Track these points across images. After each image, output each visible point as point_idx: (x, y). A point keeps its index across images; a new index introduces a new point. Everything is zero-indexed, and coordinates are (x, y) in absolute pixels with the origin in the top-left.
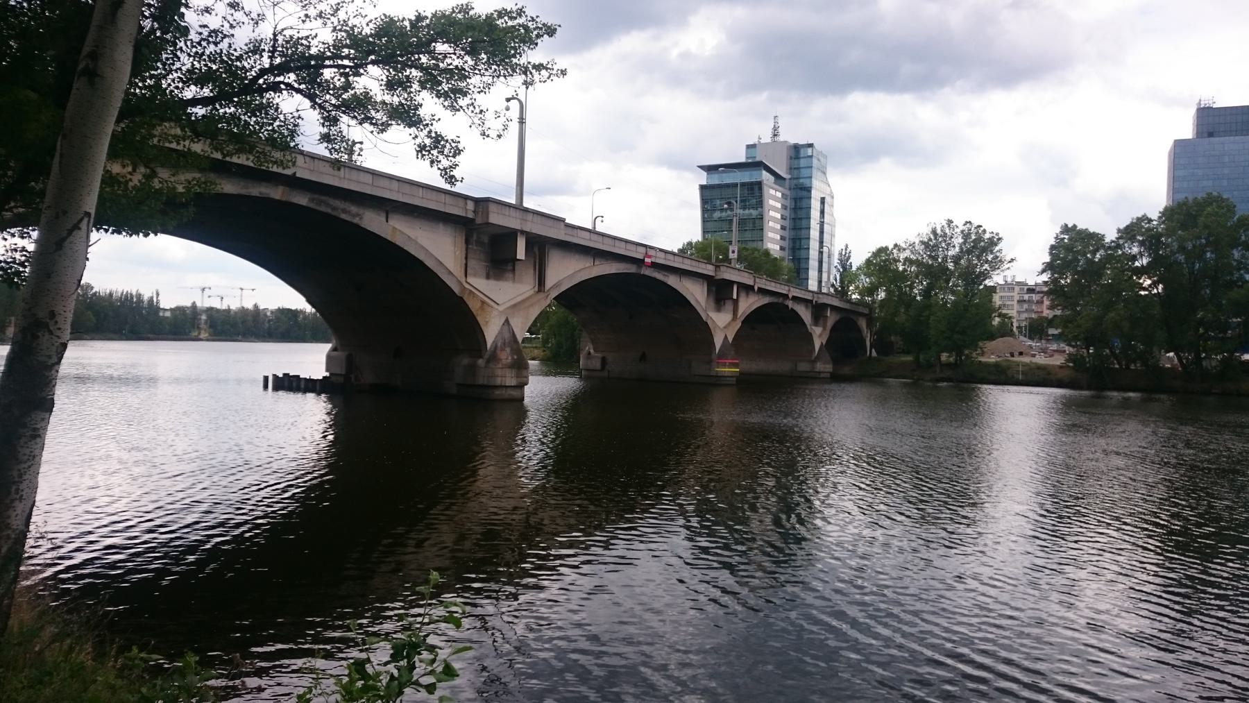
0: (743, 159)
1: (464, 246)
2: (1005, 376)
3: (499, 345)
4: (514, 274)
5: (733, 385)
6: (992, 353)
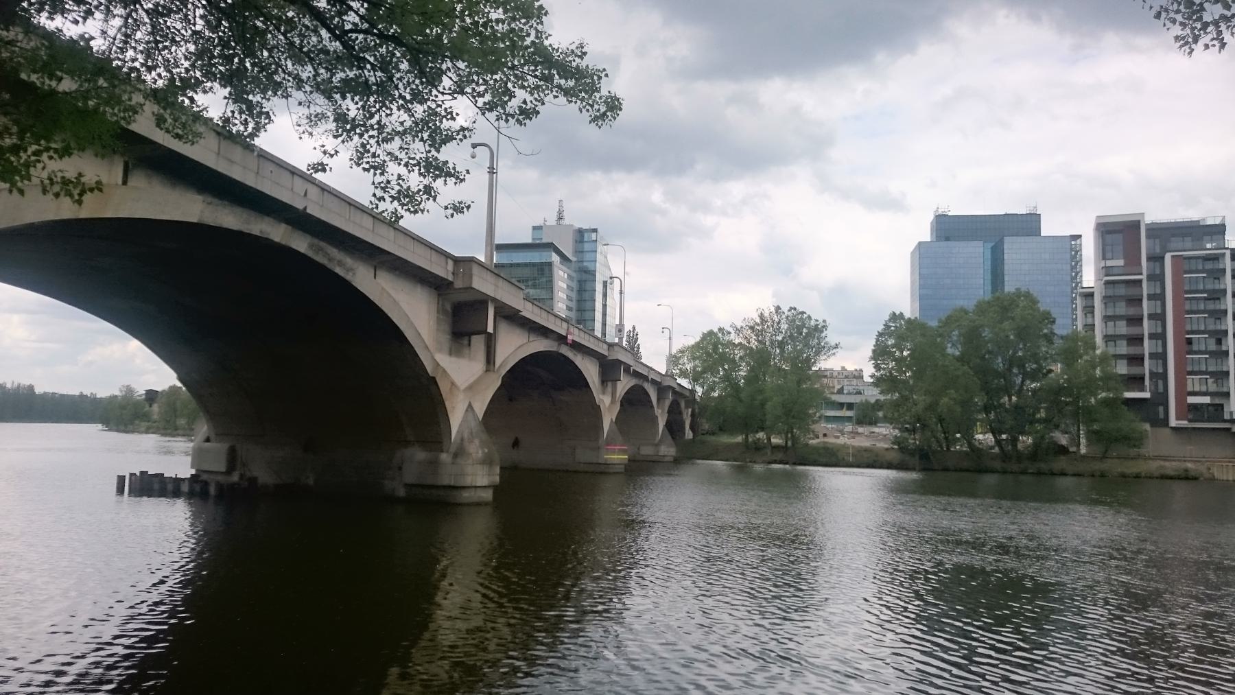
0: (529, 240)
2: (833, 458)
3: (466, 436)
4: (470, 349)
5: (622, 473)
6: (883, 434)
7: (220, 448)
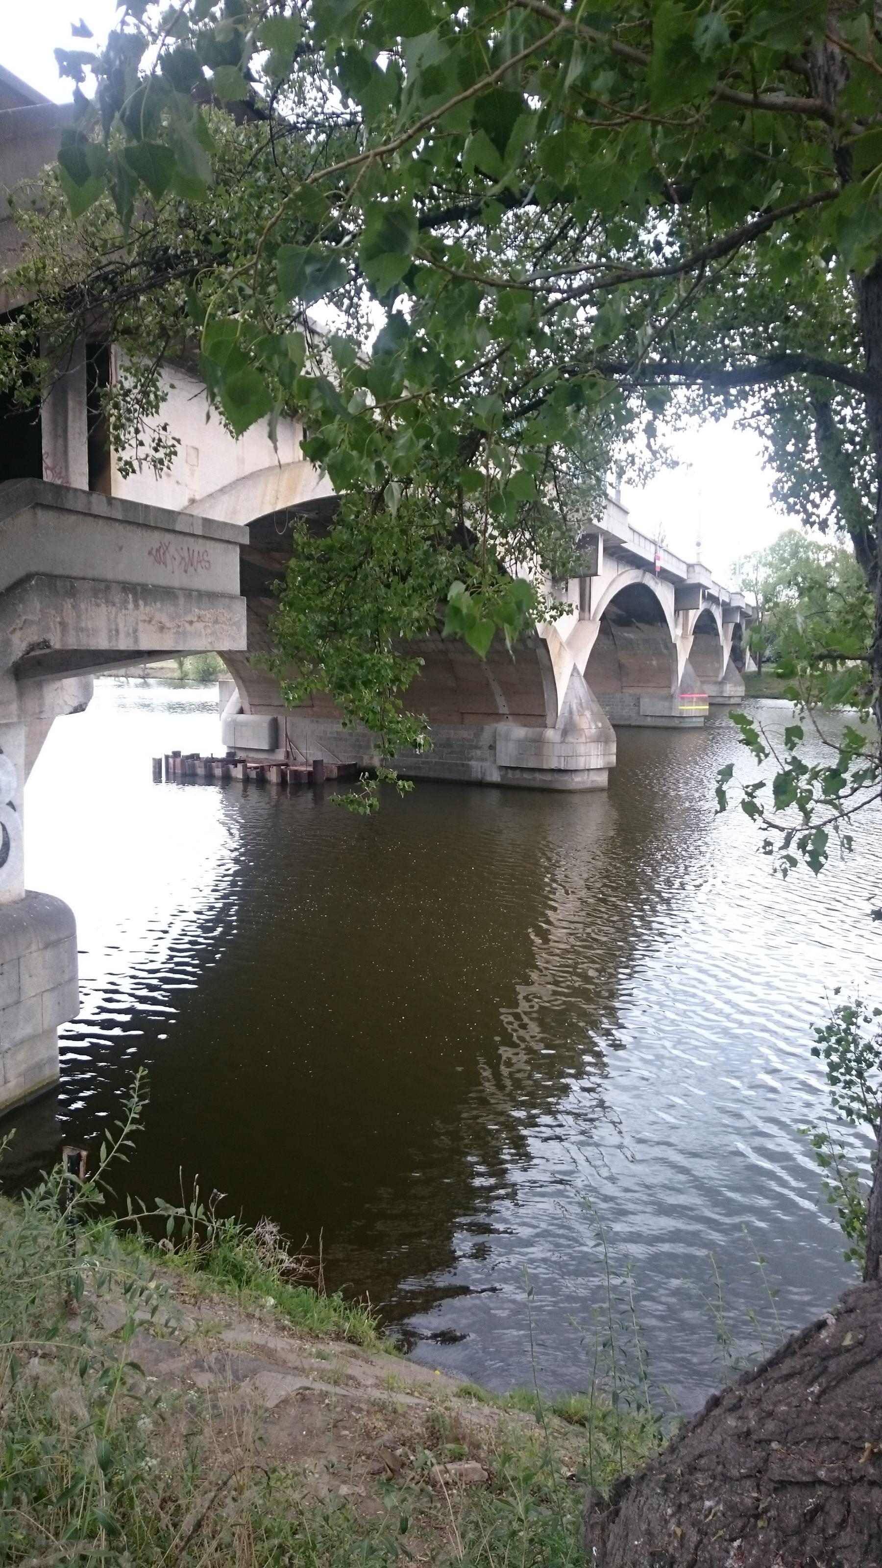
3: (574, 707)
7: (259, 722)
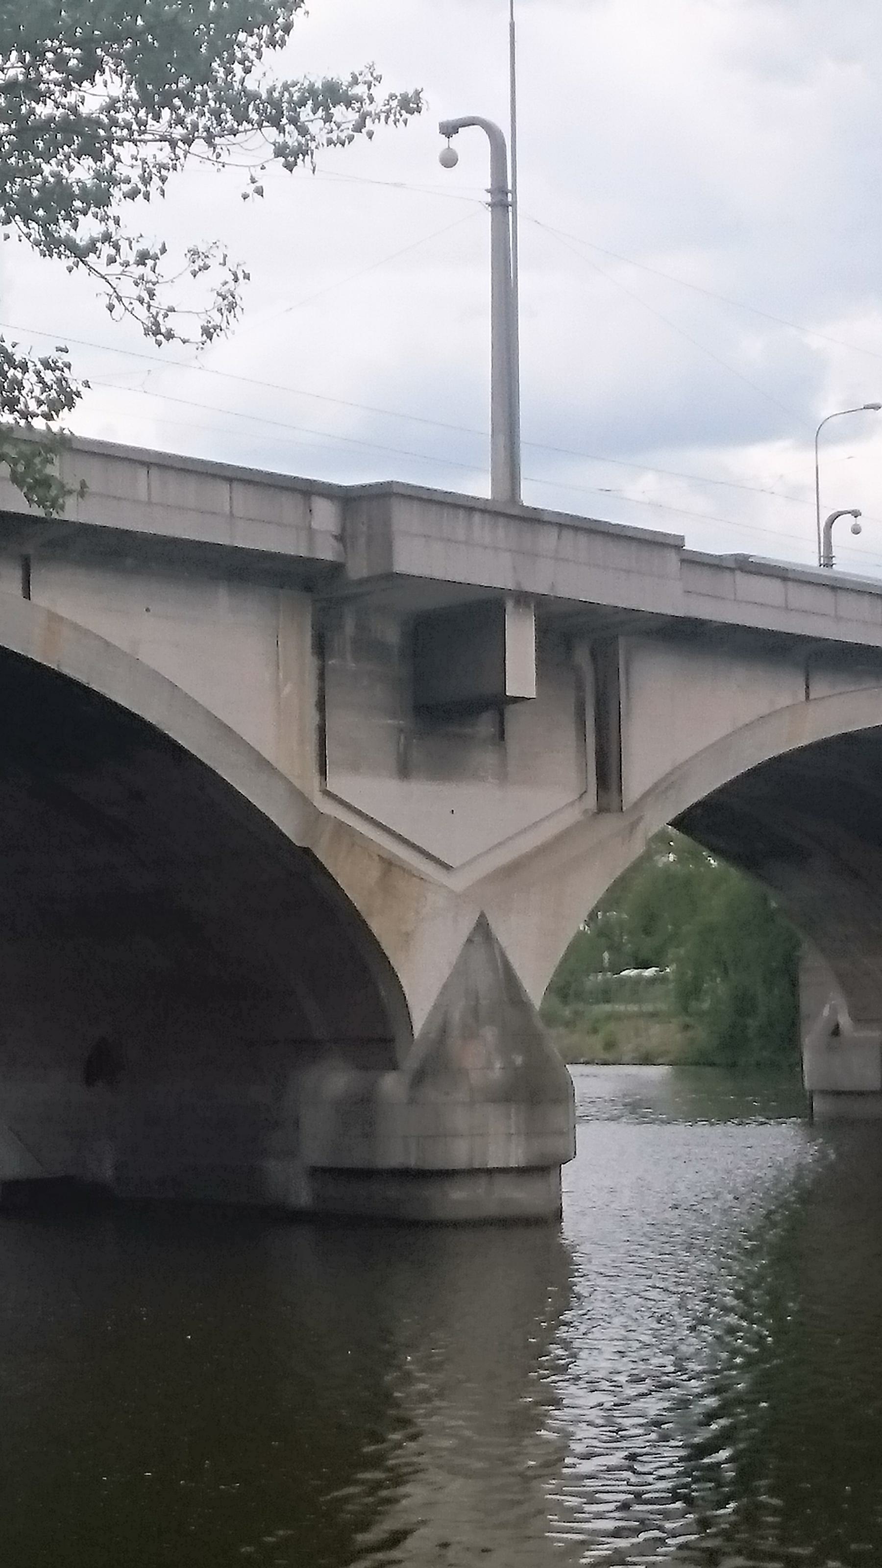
1: (311, 662)
3: (456, 1017)
